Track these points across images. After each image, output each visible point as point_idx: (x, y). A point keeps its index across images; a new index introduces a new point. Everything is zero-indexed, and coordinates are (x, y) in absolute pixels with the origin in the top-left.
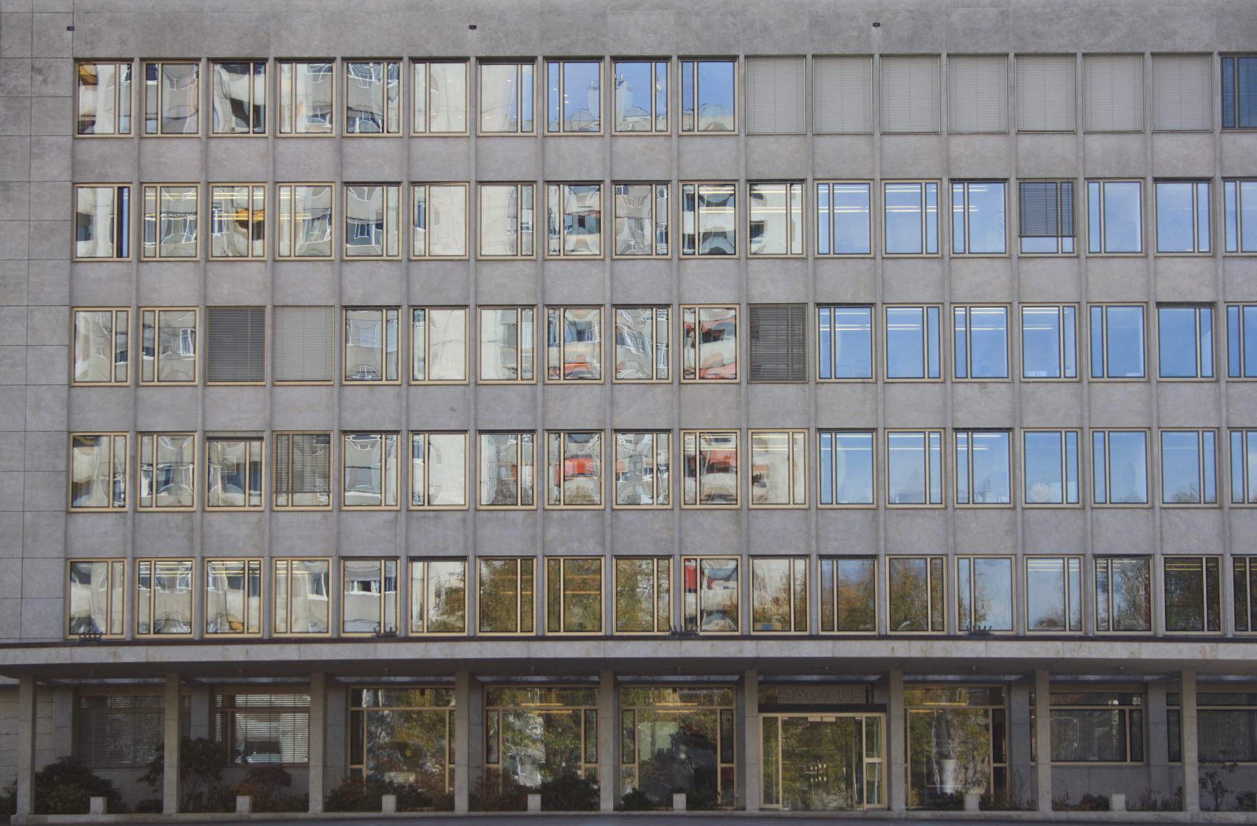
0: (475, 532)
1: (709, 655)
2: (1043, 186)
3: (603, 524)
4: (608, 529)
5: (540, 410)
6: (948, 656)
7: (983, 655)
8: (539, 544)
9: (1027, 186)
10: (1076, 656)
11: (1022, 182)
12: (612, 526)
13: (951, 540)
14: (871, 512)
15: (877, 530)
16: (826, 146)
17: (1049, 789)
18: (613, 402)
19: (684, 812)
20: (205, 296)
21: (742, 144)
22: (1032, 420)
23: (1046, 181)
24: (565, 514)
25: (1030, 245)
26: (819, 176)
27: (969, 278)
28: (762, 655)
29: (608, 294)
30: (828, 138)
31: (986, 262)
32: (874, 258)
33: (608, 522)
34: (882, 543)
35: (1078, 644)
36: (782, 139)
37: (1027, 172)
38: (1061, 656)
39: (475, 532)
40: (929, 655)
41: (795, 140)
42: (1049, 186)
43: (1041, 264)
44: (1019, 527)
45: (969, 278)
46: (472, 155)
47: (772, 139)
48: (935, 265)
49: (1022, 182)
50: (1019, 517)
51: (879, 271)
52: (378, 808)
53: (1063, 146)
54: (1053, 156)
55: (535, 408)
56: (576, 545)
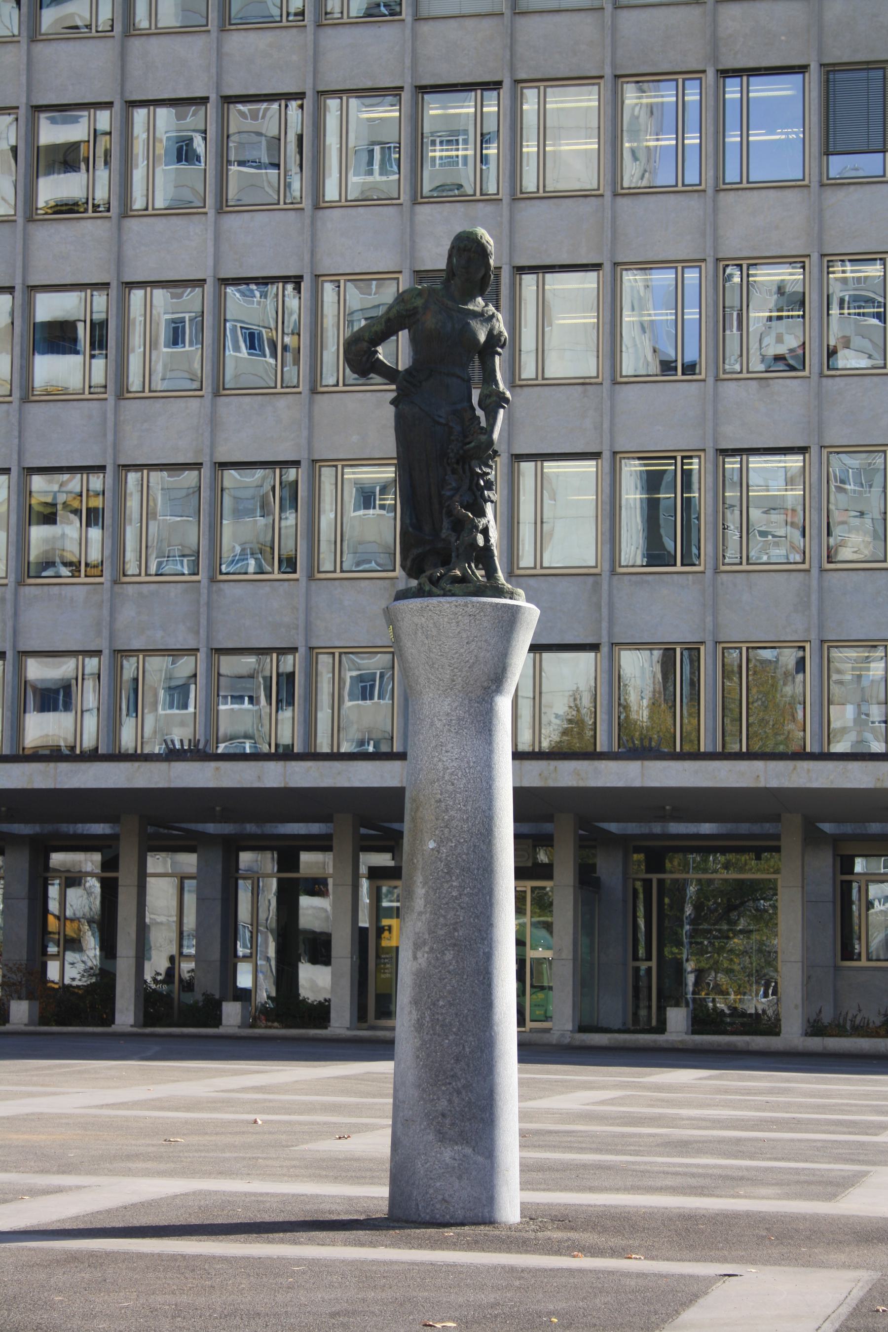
0: (16, 614)
1: (211, 784)
2: (863, 74)
3: (198, 602)
4: (203, 610)
5: (110, 437)
6: (582, 784)
7: (637, 784)
8: (105, 633)
9: (839, 76)
10: (787, 784)
11: (830, 70)
12: (209, 604)
13: (709, 619)
14: (591, 580)
15: (599, 607)
16: (532, 29)
17: (799, 1001)
18: (214, 422)
19: (235, 1031)
21: (408, 32)
22: (836, 435)
23: (868, 66)
24: (145, 589)
25: (838, 165)
26: (522, 76)
27: (744, 223)
28: (292, 784)
29: (210, 262)
30: (537, 18)
31: (772, 193)
32: (823, 255)
33: (204, 599)
34: (605, 625)
35: (790, 764)
36: (470, 23)
37: (839, 54)
38: (762, 784)
39: (16, 614)
40: (551, 784)
41: (486, 23)
42: (872, 74)
43: (855, 194)
44: (814, 597)
45: (744, 223)
46: (23, 66)
47: (453, 23)
48: (694, 202)
49: (830, 70)
50: (814, 583)
51: (608, 214)
52: (217, 1021)
55: (105, 435)
56: (159, 634)
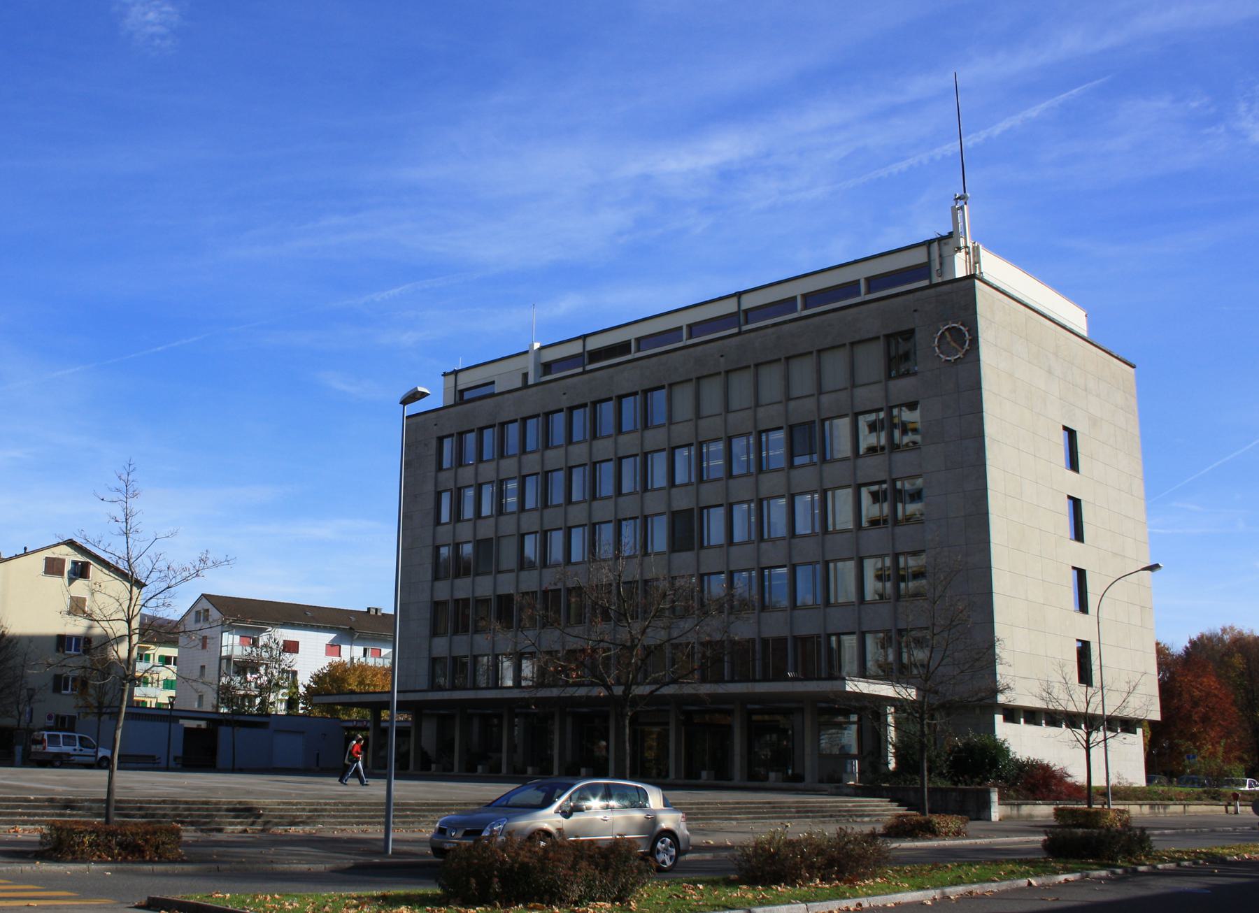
20: (669, 505)
53: (810, 404)
54: (803, 410)
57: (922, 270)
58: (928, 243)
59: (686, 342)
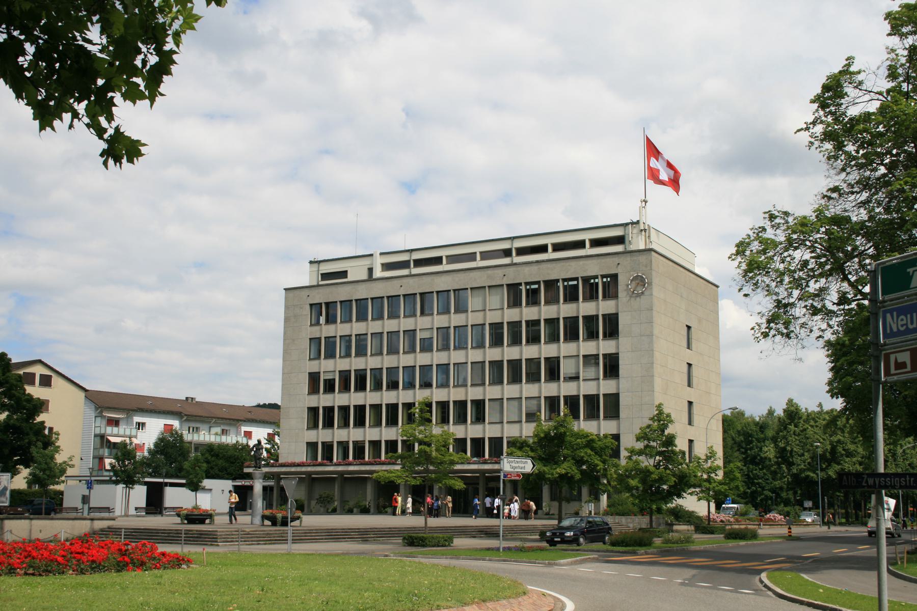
57: (620, 240)
58: (625, 225)
59: (480, 263)
